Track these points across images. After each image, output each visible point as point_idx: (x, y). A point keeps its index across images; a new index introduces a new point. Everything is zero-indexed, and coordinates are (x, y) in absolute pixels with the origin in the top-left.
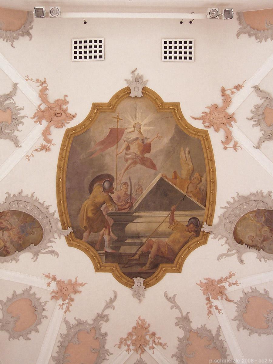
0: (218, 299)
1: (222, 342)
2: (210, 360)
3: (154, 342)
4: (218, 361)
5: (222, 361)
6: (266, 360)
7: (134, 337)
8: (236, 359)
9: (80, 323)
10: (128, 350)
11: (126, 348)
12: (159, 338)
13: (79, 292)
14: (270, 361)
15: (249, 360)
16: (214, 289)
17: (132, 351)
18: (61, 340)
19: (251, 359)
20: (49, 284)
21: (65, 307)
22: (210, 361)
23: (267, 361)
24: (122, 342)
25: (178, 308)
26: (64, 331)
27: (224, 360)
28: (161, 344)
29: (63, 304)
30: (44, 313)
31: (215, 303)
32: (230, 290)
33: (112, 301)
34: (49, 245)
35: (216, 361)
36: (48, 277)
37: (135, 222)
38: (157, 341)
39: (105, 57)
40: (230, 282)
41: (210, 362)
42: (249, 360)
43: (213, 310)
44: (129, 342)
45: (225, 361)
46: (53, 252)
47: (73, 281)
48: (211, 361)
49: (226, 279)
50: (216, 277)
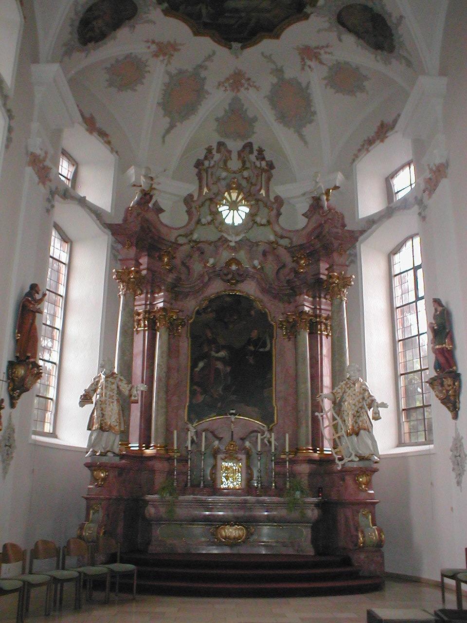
0: (312, 61)
1: (309, 94)
3: (249, 84)
7: (231, 81)
9: (181, 72)
10: (226, 90)
11: (224, 89)
12: (254, 82)
13: (179, 50)
16: (308, 53)
17: (229, 91)
18: (165, 88)
20: (149, 47)
21: (165, 62)
24: (220, 84)
25: (274, 62)
26: (167, 80)
28: (255, 87)
29: (164, 59)
30: (147, 69)
31: (308, 63)
32: (324, 57)
33: (210, 56)
34: (144, 16)
36: (147, 41)
37: (175, 195)
38: (251, 84)
43: (307, 68)
44: (226, 85)
46: (148, 22)
47: (172, 42)
49: (323, 47)
50: (313, 44)
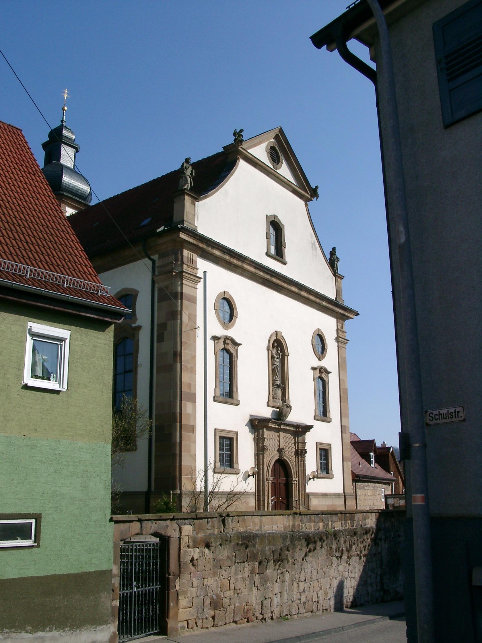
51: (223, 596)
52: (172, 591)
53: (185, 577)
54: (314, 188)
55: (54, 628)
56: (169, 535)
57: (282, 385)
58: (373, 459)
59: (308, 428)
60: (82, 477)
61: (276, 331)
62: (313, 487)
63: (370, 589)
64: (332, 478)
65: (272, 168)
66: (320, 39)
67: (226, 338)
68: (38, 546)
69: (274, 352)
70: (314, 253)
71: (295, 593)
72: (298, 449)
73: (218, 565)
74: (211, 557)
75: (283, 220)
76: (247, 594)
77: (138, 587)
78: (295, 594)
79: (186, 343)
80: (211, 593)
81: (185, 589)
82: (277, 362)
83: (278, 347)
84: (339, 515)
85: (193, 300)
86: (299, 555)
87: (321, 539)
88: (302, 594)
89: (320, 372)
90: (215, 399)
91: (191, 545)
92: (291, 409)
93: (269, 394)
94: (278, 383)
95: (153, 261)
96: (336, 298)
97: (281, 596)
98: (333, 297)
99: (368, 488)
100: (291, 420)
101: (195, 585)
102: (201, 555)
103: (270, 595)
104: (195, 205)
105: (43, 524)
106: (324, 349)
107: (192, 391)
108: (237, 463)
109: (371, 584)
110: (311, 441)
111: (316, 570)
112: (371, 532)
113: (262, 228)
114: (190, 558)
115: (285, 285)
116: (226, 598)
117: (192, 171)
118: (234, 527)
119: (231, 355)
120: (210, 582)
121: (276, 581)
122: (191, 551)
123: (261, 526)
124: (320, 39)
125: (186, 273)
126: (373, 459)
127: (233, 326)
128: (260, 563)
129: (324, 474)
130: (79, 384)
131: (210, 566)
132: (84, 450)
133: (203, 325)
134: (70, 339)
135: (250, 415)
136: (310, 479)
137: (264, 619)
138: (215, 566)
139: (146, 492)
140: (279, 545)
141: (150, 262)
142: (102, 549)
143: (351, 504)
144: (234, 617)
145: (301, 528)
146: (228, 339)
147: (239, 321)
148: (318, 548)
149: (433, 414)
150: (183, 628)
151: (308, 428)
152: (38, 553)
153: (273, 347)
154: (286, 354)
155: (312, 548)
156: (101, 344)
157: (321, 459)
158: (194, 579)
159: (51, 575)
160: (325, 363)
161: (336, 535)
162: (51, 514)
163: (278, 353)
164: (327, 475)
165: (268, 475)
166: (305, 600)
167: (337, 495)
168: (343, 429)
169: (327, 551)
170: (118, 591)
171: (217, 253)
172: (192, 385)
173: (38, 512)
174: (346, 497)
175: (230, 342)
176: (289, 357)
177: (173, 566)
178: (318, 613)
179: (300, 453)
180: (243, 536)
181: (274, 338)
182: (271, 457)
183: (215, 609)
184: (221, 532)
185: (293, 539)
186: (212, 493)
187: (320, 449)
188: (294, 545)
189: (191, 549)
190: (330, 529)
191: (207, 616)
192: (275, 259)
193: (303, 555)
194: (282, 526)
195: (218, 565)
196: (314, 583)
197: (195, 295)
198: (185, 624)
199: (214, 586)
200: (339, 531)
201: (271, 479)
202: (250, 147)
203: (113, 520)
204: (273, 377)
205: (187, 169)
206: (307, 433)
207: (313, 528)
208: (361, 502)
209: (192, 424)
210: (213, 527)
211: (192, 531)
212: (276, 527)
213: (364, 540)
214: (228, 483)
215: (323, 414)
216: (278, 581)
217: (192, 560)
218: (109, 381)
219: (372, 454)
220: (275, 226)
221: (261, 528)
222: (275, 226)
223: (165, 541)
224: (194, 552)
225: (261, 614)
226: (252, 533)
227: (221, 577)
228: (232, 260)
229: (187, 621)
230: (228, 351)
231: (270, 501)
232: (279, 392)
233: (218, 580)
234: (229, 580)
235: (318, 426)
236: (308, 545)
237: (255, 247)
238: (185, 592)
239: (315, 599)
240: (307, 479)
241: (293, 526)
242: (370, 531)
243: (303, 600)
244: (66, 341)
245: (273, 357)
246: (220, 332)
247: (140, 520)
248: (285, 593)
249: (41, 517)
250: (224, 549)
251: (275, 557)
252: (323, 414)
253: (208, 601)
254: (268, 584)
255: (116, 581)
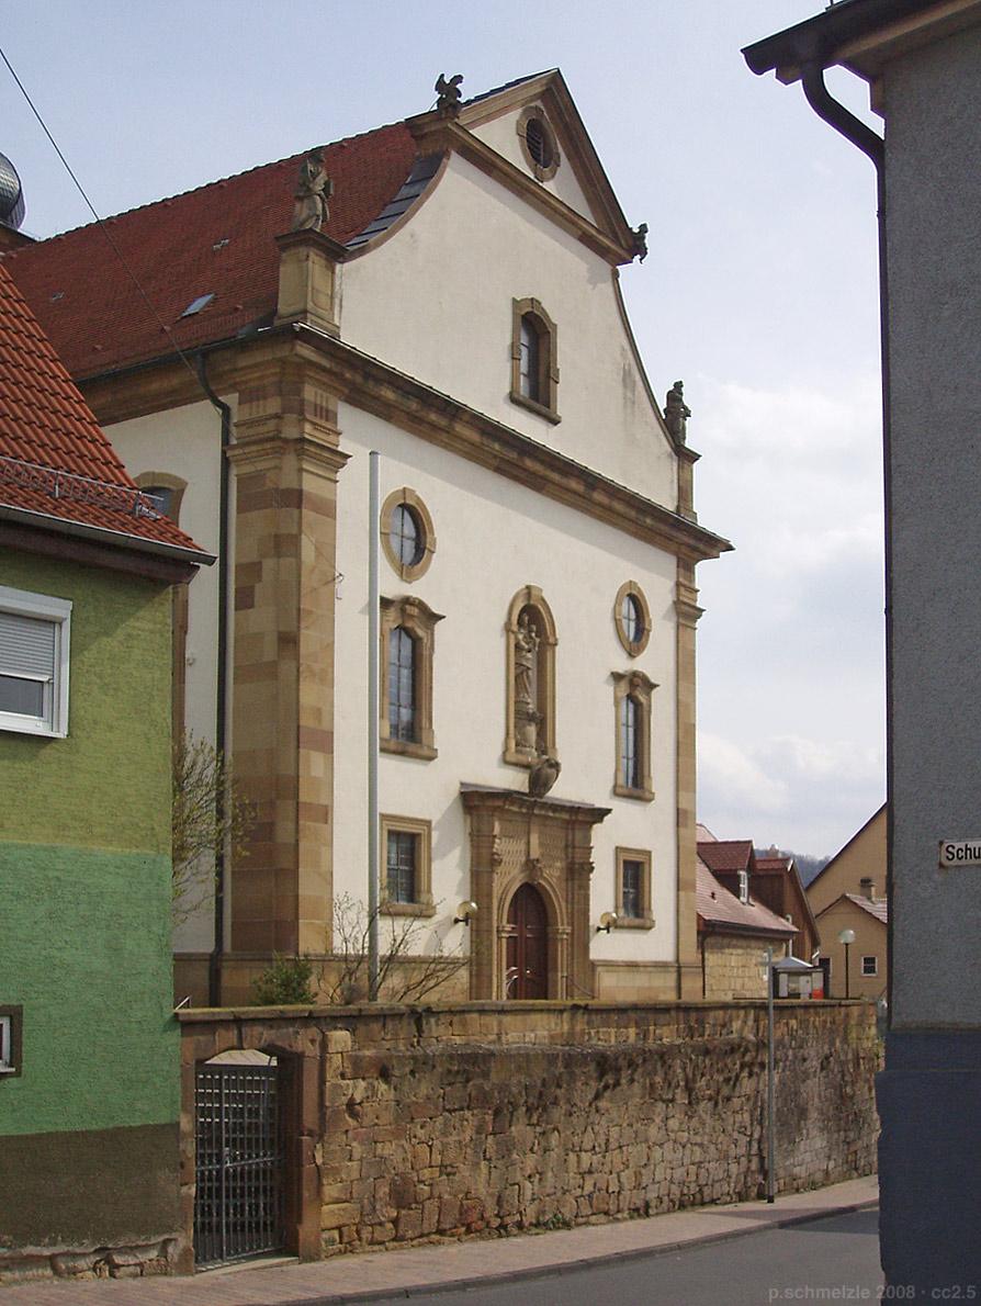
2: (771, 1291)
4: (946, 1294)
5: (810, 1293)
6: (956, 1290)
8: (858, 1287)
14: (971, 1294)
15: (900, 1294)
19: (906, 1286)
22: (773, 1294)
23: (961, 1294)
27: (818, 1291)
35: (789, 1293)
39: (897, 881)
40: (681, 598)
41: (771, 1297)
42: (900, 1294)
45: (826, 1295)
48: (774, 1293)
51: (416, 1179)
52: (308, 1167)
53: (336, 1140)
54: (636, 230)
55: (60, 1238)
56: (300, 1050)
57: (538, 715)
58: (744, 886)
59: (600, 814)
60: (108, 927)
61: (528, 587)
62: (604, 947)
63: (734, 1168)
64: (650, 928)
65: (532, 177)
66: (760, 56)
67: (407, 601)
68: (18, 1074)
69: (521, 637)
70: (629, 395)
71: (572, 1174)
72: (573, 863)
73: (406, 1113)
74: (392, 1097)
75: (554, 312)
76: (467, 1174)
77: (234, 1159)
78: (572, 1179)
79: (310, 612)
80: (389, 1173)
81: (337, 1165)
82: (530, 659)
83: (531, 623)
84: (673, 1013)
85: (328, 509)
86: (584, 1092)
87: (631, 1064)
88: (587, 1177)
89: (633, 685)
90: (382, 750)
91: (349, 1071)
92: (558, 771)
93: (507, 734)
94: (532, 707)
95: (226, 409)
96: (678, 507)
97: (540, 1180)
98: (668, 502)
99: (731, 950)
100: (558, 796)
101: (356, 1155)
102: (370, 1093)
103: (519, 1178)
104: (333, 272)
105: (26, 1029)
106: (641, 631)
107: (325, 726)
108: (429, 891)
109: (737, 1159)
110: (603, 844)
111: (617, 1128)
112: (742, 1049)
113: (501, 331)
114: (345, 1100)
115: (556, 477)
116: (423, 1182)
117: (327, 184)
118: (443, 1037)
119: (416, 642)
120: (387, 1149)
121: (531, 1150)
122: (348, 1085)
123: (499, 1035)
124: (760, 56)
125: (311, 442)
126: (744, 886)
127: (423, 571)
128: (497, 1113)
129: (631, 920)
130: (95, 722)
131: (387, 1117)
132: (111, 869)
133: (355, 576)
134: (72, 621)
135: (462, 784)
136: (599, 929)
137: (503, 1226)
138: (398, 1118)
139: (211, 955)
140: (539, 1072)
141: (215, 413)
142: (157, 1080)
143: (691, 986)
144: (438, 1221)
145: (586, 1037)
146: (412, 604)
147: (436, 563)
148: (623, 1081)
149: (953, 847)
150: (331, 1242)
151: (600, 814)
152: (19, 1089)
153: (520, 623)
154: (551, 640)
155: (611, 1082)
156: (143, 631)
157: (625, 885)
158: (354, 1144)
159: (49, 1134)
160: (641, 664)
161: (664, 1055)
162: (44, 1007)
163: (531, 637)
164: (637, 921)
165: (500, 919)
166: (592, 1189)
167: (661, 966)
168: (683, 817)
169: (644, 1087)
170: (193, 1167)
171: (389, 394)
172: (324, 712)
173: (15, 1003)
174: (683, 970)
175: (415, 611)
176: (557, 648)
177: (310, 1118)
178: (619, 1216)
179: (579, 871)
180: (462, 1055)
181: (520, 605)
182: (507, 880)
183: (399, 1207)
184: (412, 1046)
185: (569, 1061)
186: (391, 959)
187: (625, 862)
188: (572, 1075)
189: (348, 1081)
190: (651, 1044)
191: (383, 1219)
192: (531, 410)
193: (590, 1097)
194: (546, 1033)
195: (406, 1113)
196: (615, 1157)
197: (333, 498)
198: (336, 1234)
199: (398, 1158)
200: (672, 1046)
201: (508, 927)
202: (474, 124)
203: (181, 1018)
204: (517, 693)
205: (314, 176)
206: (595, 826)
207: (613, 1039)
208: (713, 981)
209: (323, 801)
210: (396, 1038)
211: (350, 1043)
212: (533, 1035)
213: (726, 1065)
214: (418, 938)
215: (635, 785)
216: (536, 1148)
217: (351, 1104)
218: (164, 715)
219: (742, 873)
220: (534, 328)
221: (499, 1038)
222: (534, 328)
223: (289, 1064)
224: (355, 1087)
225: (497, 1216)
226: (480, 1047)
227: (413, 1139)
228: (425, 413)
229: (339, 1228)
230: (409, 633)
231: (504, 978)
232: (532, 730)
233: (407, 1146)
234: (430, 1147)
235: (622, 810)
236: (601, 1075)
237: (482, 382)
238: (336, 1171)
239: (613, 1188)
240: (592, 930)
241: (572, 1033)
242: (740, 1046)
243: (588, 1188)
244: (64, 624)
245: (518, 646)
246: (391, 585)
247: (525, 1043)
248: (550, 1174)
249: (21, 1014)
250: (419, 1081)
251: (531, 1100)
252: (635, 785)
253: (384, 1190)
254: (515, 1156)
255: (190, 1148)
